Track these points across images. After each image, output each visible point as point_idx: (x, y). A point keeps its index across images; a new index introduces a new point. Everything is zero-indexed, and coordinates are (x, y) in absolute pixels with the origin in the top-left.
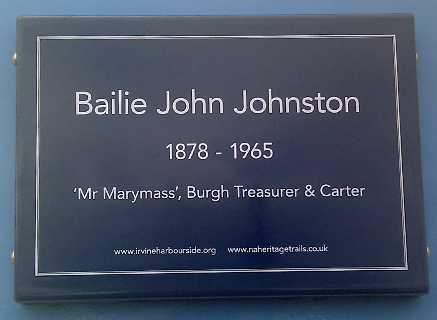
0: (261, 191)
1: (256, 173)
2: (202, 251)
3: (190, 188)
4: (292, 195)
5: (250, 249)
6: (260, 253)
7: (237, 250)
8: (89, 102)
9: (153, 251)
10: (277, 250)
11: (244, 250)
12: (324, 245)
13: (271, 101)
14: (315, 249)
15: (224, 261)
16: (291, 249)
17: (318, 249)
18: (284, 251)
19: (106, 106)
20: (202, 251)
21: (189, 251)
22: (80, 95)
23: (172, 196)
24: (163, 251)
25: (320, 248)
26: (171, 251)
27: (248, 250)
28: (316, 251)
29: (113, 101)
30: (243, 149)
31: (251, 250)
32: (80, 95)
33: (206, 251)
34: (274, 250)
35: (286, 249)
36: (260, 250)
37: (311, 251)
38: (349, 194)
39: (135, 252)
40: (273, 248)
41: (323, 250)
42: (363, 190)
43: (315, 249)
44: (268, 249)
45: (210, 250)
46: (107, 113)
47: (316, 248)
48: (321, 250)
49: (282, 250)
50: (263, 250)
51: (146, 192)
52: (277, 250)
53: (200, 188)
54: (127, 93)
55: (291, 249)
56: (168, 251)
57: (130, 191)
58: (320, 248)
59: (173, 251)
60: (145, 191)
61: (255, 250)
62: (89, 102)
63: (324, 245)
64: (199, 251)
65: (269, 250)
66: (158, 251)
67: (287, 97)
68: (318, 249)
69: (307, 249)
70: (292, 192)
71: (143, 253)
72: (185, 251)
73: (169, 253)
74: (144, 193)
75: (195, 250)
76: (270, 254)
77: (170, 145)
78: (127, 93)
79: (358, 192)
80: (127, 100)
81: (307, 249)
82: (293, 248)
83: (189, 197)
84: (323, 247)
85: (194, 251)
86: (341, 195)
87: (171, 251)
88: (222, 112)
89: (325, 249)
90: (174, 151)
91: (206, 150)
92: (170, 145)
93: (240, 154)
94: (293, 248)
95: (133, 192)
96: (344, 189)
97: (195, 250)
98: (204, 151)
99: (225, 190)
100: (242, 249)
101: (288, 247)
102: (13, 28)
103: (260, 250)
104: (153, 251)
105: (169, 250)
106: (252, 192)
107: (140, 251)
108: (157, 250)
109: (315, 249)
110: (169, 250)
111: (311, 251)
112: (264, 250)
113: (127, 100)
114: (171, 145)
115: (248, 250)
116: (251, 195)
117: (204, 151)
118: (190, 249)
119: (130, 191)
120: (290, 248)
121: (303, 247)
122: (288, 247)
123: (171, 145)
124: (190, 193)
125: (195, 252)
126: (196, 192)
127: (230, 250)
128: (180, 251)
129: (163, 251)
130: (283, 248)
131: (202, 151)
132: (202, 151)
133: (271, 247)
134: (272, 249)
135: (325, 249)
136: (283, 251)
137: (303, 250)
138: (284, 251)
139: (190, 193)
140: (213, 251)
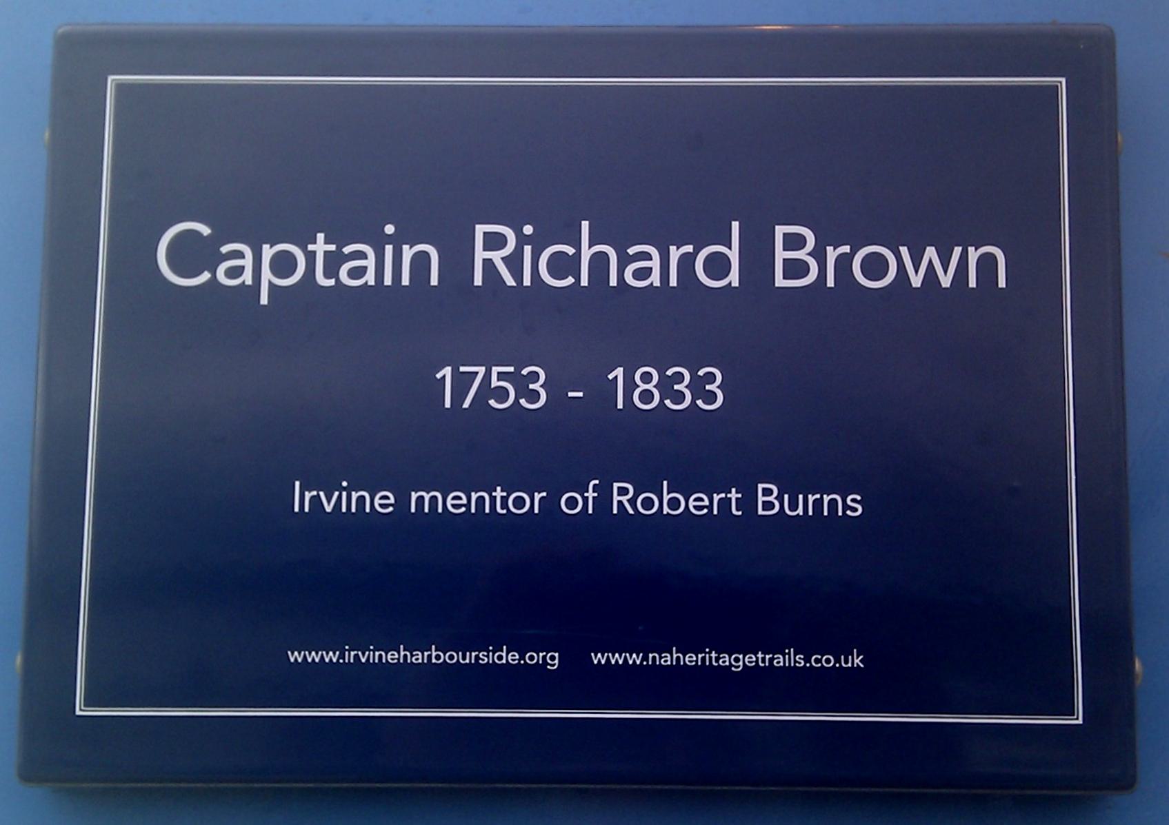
2: (522, 657)
3: (764, 489)
4: (463, 509)
6: (678, 669)
8: (809, 254)
9: (392, 657)
10: (726, 660)
11: (635, 659)
14: (827, 661)
15: (581, 684)
16: (764, 660)
17: (838, 660)
19: (370, 263)
20: (522, 657)
23: (855, 510)
26: (438, 657)
27: (645, 658)
29: (389, 249)
31: (654, 658)
34: (717, 659)
35: (750, 660)
36: (678, 658)
38: (502, 508)
39: (342, 656)
40: (714, 655)
42: (542, 498)
45: (544, 657)
46: (657, 284)
48: (846, 662)
49: (737, 660)
50: (389, 657)
51: (427, 497)
52: (726, 660)
53: (791, 487)
54: (528, 230)
55: (764, 660)
56: (430, 657)
57: (315, 493)
59: (444, 657)
60: (423, 493)
61: (667, 660)
62: (809, 254)
64: (513, 658)
65: (703, 659)
66: (405, 656)
69: (807, 660)
70: (464, 501)
71: (363, 660)
72: (477, 657)
73: (434, 661)
74: (422, 497)
75: (504, 654)
76: (703, 670)
77: (619, 372)
78: (528, 230)
79: (706, 503)
80: (528, 249)
83: (760, 512)
85: (500, 658)
87: (438, 657)
88: (1002, 283)
90: (630, 386)
92: (619, 372)
95: (322, 494)
96: (723, 495)
99: (672, 495)
102: (45, 57)
103: (678, 658)
104: (392, 657)
105: (434, 654)
106: (701, 500)
107: (356, 656)
108: (402, 653)
109: (827, 661)
110: (434, 654)
112: (690, 659)
113: (528, 249)
114: (449, 369)
115: (645, 658)
118: (489, 652)
119: (315, 493)
120: (760, 655)
123: (449, 369)
124: (764, 502)
125: (504, 661)
126: (780, 498)
127: (598, 658)
129: (419, 657)
133: (710, 653)
134: (711, 658)
136: (741, 663)
137: (795, 662)
139: (764, 502)
140: (553, 658)
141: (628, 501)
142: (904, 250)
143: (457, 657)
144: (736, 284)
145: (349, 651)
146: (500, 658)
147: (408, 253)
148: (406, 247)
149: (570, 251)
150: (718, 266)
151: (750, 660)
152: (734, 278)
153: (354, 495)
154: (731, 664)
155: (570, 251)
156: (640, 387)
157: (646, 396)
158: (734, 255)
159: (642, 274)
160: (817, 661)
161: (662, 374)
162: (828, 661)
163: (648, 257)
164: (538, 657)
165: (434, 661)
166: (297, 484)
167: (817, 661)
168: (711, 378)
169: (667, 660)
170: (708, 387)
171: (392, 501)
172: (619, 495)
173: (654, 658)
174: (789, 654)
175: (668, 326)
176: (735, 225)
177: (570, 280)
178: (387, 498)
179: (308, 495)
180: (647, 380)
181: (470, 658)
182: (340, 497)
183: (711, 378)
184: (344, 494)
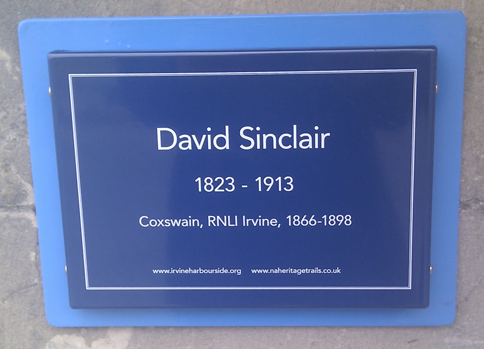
0: (185, 221)
1: (276, 204)
3: (211, 218)
5: (271, 270)
6: (280, 274)
7: (161, 271)
10: (295, 271)
11: (266, 271)
12: (338, 268)
13: (323, 137)
14: (329, 271)
15: (248, 279)
16: (308, 271)
17: (332, 271)
18: (302, 273)
19: (310, 140)
21: (218, 271)
22: (161, 131)
24: (195, 271)
25: (334, 270)
26: (202, 271)
27: (269, 271)
28: (330, 272)
29: (316, 135)
30: (267, 183)
31: (272, 271)
32: (161, 131)
33: (232, 271)
34: (293, 271)
35: (303, 271)
36: (280, 271)
37: (326, 272)
39: (170, 271)
40: (292, 270)
41: (336, 272)
43: (329, 271)
44: (287, 270)
47: (330, 270)
48: (335, 271)
49: (299, 271)
52: (295, 271)
55: (308, 271)
56: (199, 271)
57: (250, 220)
58: (334, 270)
61: (276, 271)
63: (338, 268)
64: (226, 271)
65: (288, 271)
66: (191, 271)
67: (264, 134)
68: (332, 271)
69: (322, 271)
72: (214, 271)
73: (200, 272)
75: (223, 270)
81: (322, 271)
82: (309, 270)
84: (337, 269)
85: (222, 271)
86: (248, 225)
87: (202, 271)
89: (338, 271)
91: (292, 183)
93: (264, 187)
94: (309, 270)
97: (223, 270)
98: (210, 184)
100: (264, 270)
101: (305, 269)
104: (186, 271)
105: (200, 270)
107: (175, 271)
109: (329, 271)
110: (200, 270)
111: (326, 272)
112: (284, 271)
115: (269, 271)
116: (273, 224)
117: (210, 184)
118: (218, 269)
119: (250, 220)
121: (318, 269)
122: (305, 269)
125: (223, 272)
127: (254, 271)
128: (210, 272)
129: (195, 271)
130: (300, 270)
131: (207, 184)
132: (207, 184)
133: (290, 269)
134: (291, 271)
135: (338, 271)
136: (300, 272)
137: (318, 271)
138: (302, 273)
140: (239, 271)
141: (214, 222)
142: (194, 136)
143: (208, 271)
144: (228, 148)
145: (173, 270)
146: (222, 271)
147: (265, 137)
148: (322, 134)
149: (290, 136)
150: (221, 142)
151: (303, 271)
152: (227, 146)
153: (263, 220)
154: (297, 273)
155: (290, 136)
156: (265, 182)
157: (209, 187)
158: (227, 138)
159: (306, 144)
160: (325, 271)
161: (214, 180)
162: (329, 271)
163: (307, 138)
164: (234, 271)
165: (200, 272)
166: (244, 217)
167: (325, 271)
168: (289, 180)
169: (276, 271)
170: (288, 183)
171: (276, 222)
172: (211, 220)
173: (272, 271)
174: (316, 269)
175: (272, 161)
176: (295, 126)
177: (290, 147)
178: (275, 221)
179: (248, 220)
180: (209, 181)
181: (212, 271)
182: (258, 221)
183: (289, 180)
184: (260, 220)
